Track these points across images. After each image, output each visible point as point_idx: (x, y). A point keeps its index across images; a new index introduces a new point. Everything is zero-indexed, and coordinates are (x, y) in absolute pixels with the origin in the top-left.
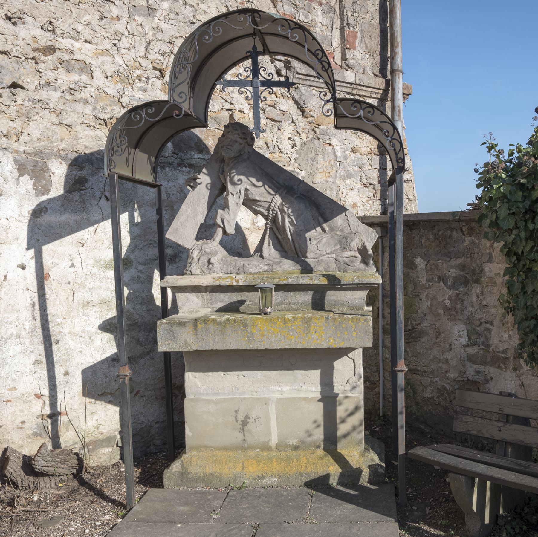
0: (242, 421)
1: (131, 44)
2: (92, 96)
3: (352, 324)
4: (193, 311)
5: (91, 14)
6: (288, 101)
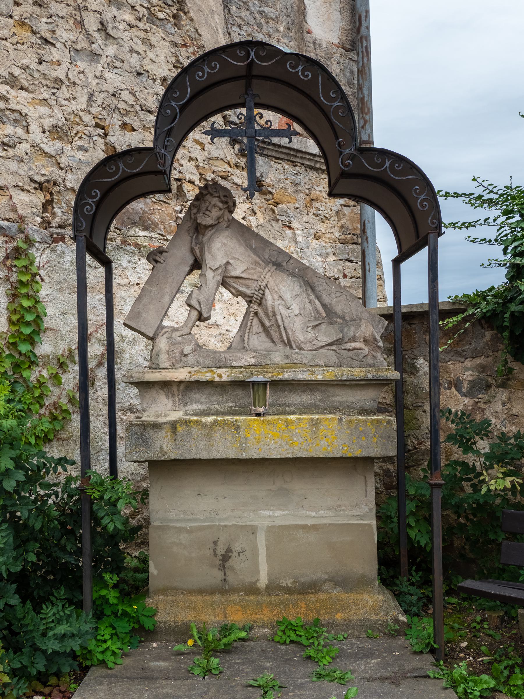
0: (222, 555)
1: (72, 94)
2: (27, 154)
3: (371, 426)
4: (161, 415)
5: (29, 56)
6: (243, 172)
